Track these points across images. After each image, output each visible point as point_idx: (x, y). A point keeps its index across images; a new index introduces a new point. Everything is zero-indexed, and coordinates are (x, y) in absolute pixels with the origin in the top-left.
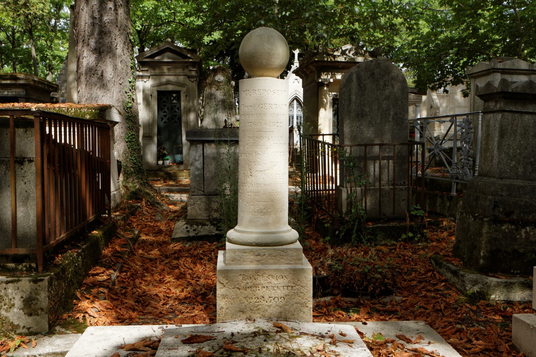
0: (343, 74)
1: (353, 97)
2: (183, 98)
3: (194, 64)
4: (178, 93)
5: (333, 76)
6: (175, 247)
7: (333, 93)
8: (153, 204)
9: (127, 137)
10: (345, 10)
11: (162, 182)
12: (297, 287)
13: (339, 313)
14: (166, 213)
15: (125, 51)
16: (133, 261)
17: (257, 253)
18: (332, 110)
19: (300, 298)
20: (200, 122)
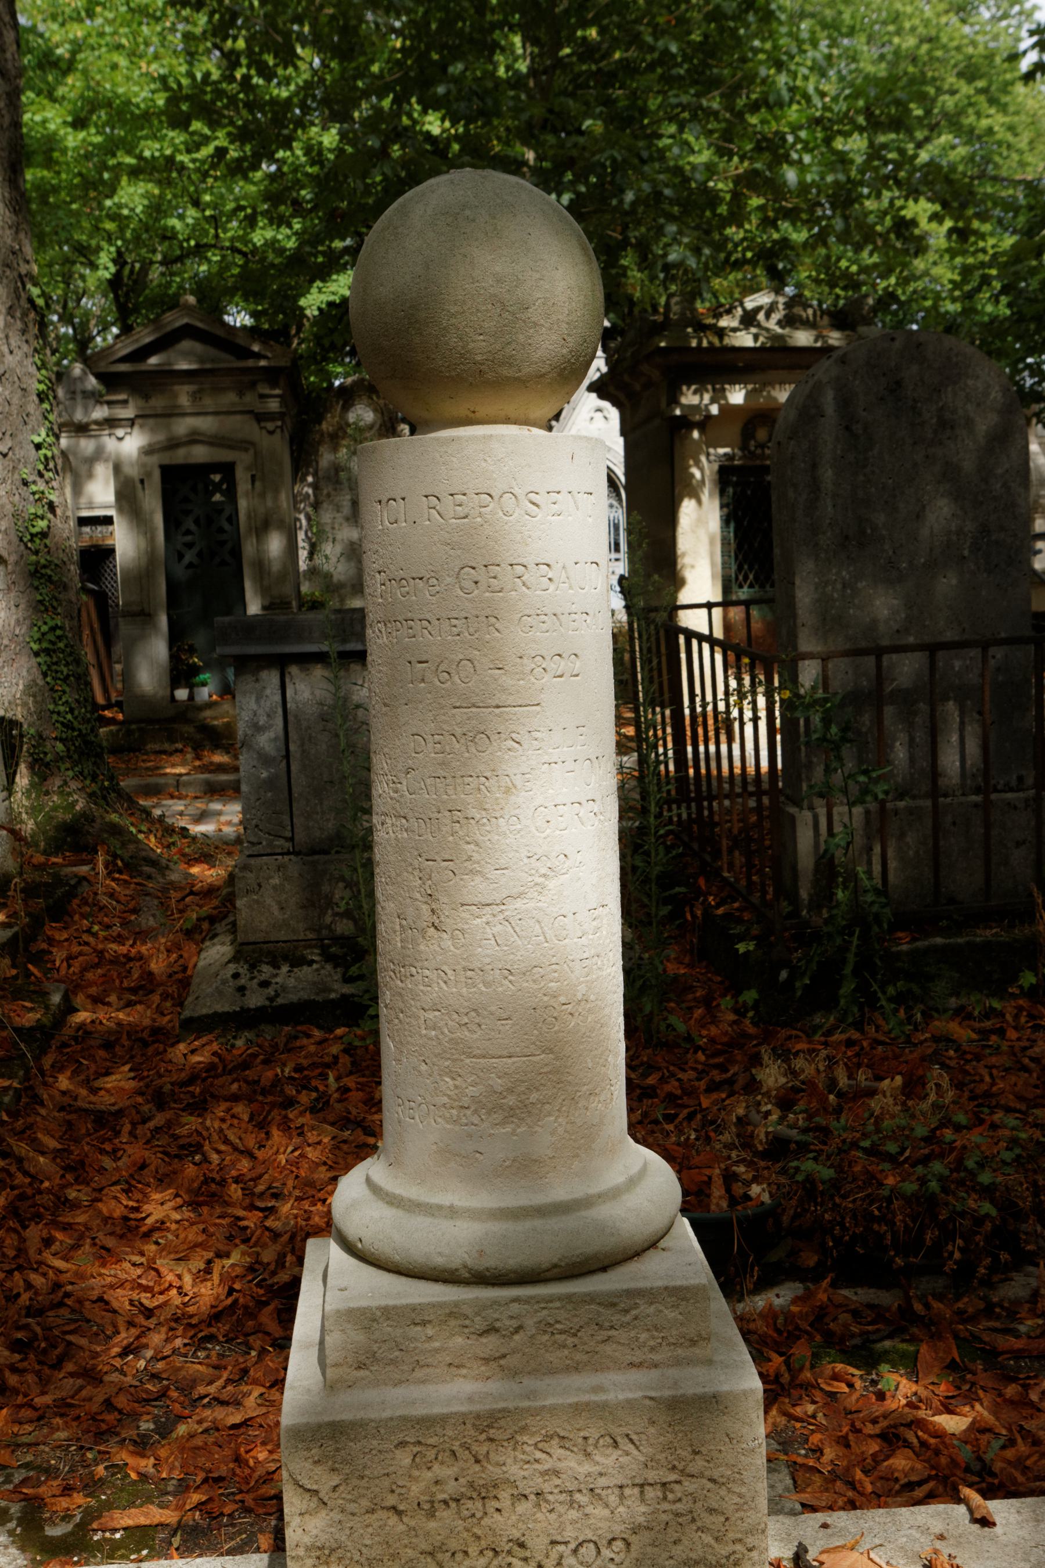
0: (750, 387)
1: (827, 475)
2: (243, 485)
3: (271, 376)
4: (228, 469)
5: (719, 396)
6: (194, 1054)
7: (721, 451)
8: (135, 865)
9: (37, 636)
10: (750, 181)
11: (189, 756)
12: (689, 1486)
13: (836, 1377)
14: (179, 895)
15: (14, 341)
16: (26, 1134)
17: (479, 1324)
18: (717, 503)
19: (708, 1539)
20: (303, 554)
